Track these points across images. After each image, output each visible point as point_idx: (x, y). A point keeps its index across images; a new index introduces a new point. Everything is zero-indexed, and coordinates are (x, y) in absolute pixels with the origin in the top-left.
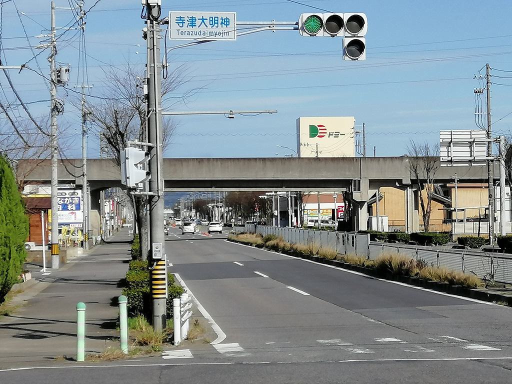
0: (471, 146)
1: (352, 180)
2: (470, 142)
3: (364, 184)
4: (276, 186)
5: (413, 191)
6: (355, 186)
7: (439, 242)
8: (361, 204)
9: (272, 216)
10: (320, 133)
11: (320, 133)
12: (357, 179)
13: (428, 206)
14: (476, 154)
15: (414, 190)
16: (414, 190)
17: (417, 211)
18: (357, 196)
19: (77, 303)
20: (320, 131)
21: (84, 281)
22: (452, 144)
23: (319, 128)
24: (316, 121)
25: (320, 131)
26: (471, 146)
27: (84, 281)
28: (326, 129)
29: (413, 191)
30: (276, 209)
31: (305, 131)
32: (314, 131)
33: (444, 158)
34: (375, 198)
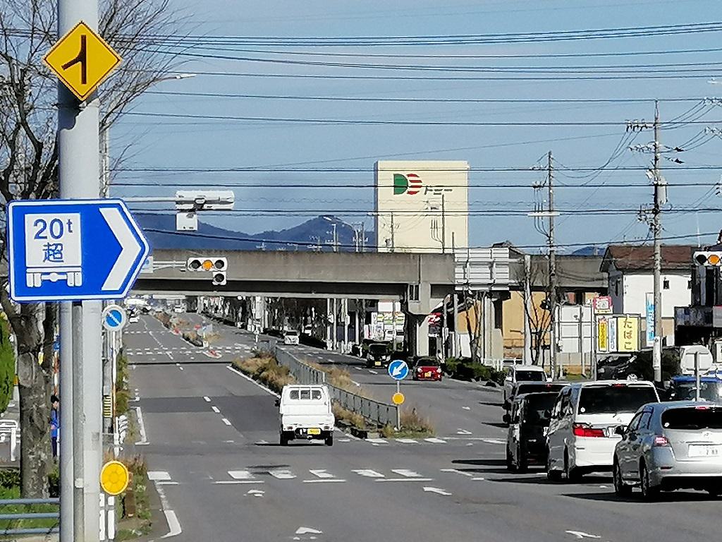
0: (491, 267)
1: (407, 284)
2: (490, 262)
3: (424, 291)
4: (297, 290)
5: (494, 302)
6: (411, 293)
7: (482, 377)
8: (421, 318)
9: (328, 323)
10: (412, 187)
11: (412, 187)
12: (414, 283)
13: (476, 329)
14: (495, 276)
15: (493, 300)
16: (493, 300)
17: (500, 330)
18: (414, 308)
19: (80, 287)
20: (410, 184)
21: (488, 211)
22: (468, 264)
23: (409, 179)
24: (405, 167)
25: (410, 184)
26: (491, 267)
27: (488, 211)
28: (420, 181)
29: (494, 302)
30: (332, 312)
31: (386, 179)
32: (400, 185)
33: (459, 281)
34: (452, 309)
